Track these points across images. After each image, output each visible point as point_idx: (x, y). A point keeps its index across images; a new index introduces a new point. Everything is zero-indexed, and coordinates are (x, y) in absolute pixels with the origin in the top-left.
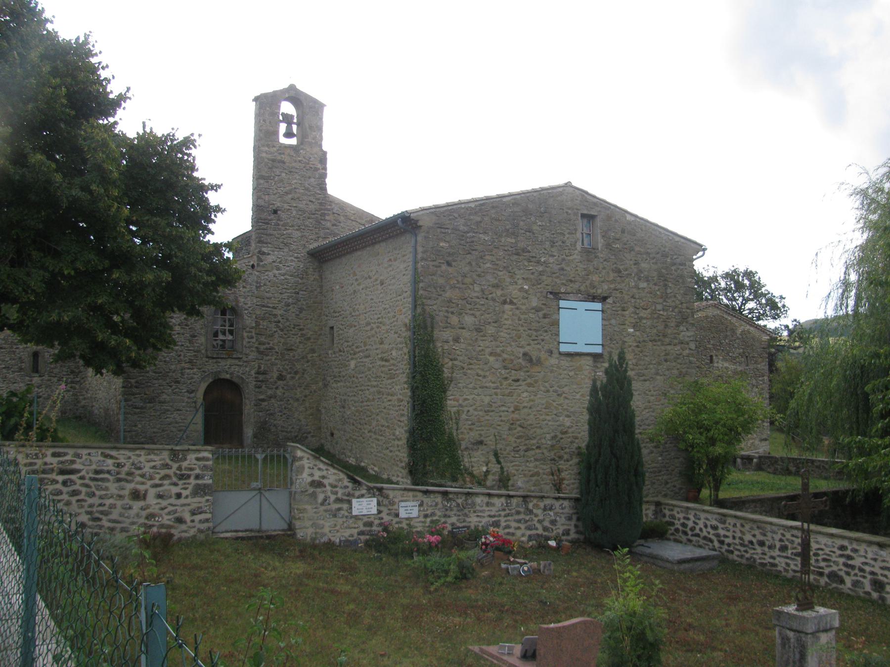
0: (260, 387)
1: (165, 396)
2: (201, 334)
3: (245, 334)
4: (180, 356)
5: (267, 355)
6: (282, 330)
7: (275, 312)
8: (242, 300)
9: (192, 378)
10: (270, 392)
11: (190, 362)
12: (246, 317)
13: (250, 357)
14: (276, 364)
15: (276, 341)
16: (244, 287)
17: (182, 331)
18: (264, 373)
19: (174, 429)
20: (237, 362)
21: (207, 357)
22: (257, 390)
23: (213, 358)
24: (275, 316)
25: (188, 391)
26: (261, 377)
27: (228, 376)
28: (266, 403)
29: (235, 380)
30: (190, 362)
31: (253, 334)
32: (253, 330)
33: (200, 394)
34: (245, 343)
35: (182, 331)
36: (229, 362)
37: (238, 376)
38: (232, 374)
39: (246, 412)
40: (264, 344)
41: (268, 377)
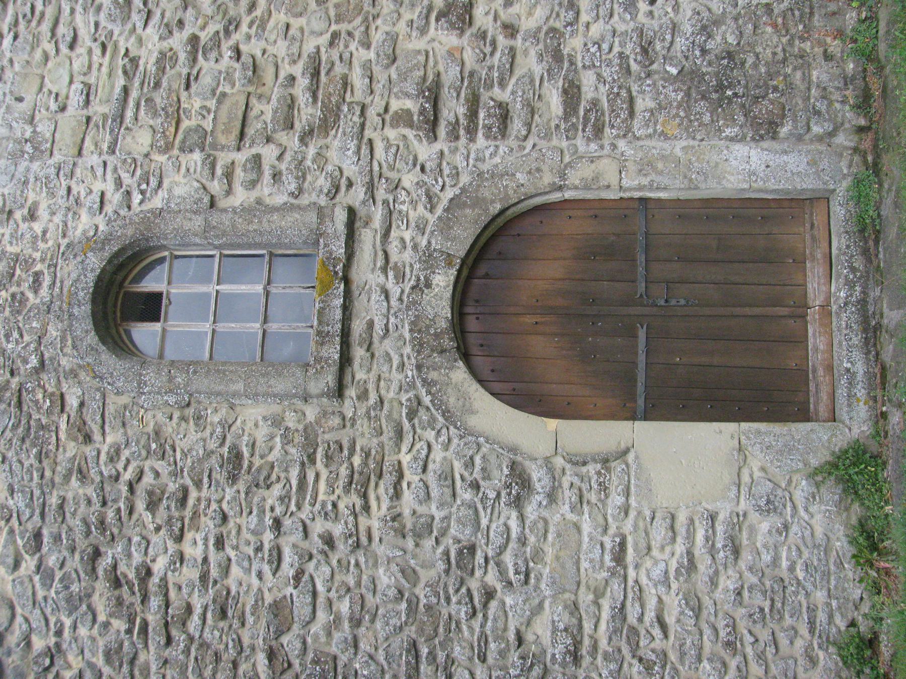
0: (504, 115)
1: (541, 629)
2: (227, 426)
3: (241, 196)
4: (329, 541)
5: (346, 83)
6: (231, 26)
7: (148, 61)
8: (84, 223)
9: (447, 477)
10: (531, 63)
11: (361, 484)
12: (157, 202)
13: (351, 169)
14: (393, 39)
15: (281, 48)
16: (32, 216)
17: (208, 523)
18: (433, 94)
19: (728, 582)
20: (368, 239)
21: (340, 392)
22: (517, 126)
23: (345, 360)
24: (165, 59)
25: (518, 503)
26: (453, 108)
27: (443, 281)
28: (588, 80)
29: (460, 244)
30: (361, 484)
31: (241, 157)
32: (223, 159)
33: (532, 434)
34: (280, 199)
35: (208, 523)
36: (365, 272)
37: (445, 225)
38: (428, 258)
39: (633, 184)
40: (291, 104)
41: (450, 75)
